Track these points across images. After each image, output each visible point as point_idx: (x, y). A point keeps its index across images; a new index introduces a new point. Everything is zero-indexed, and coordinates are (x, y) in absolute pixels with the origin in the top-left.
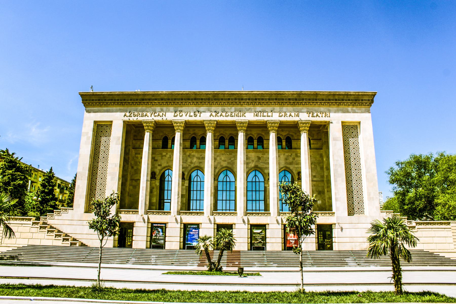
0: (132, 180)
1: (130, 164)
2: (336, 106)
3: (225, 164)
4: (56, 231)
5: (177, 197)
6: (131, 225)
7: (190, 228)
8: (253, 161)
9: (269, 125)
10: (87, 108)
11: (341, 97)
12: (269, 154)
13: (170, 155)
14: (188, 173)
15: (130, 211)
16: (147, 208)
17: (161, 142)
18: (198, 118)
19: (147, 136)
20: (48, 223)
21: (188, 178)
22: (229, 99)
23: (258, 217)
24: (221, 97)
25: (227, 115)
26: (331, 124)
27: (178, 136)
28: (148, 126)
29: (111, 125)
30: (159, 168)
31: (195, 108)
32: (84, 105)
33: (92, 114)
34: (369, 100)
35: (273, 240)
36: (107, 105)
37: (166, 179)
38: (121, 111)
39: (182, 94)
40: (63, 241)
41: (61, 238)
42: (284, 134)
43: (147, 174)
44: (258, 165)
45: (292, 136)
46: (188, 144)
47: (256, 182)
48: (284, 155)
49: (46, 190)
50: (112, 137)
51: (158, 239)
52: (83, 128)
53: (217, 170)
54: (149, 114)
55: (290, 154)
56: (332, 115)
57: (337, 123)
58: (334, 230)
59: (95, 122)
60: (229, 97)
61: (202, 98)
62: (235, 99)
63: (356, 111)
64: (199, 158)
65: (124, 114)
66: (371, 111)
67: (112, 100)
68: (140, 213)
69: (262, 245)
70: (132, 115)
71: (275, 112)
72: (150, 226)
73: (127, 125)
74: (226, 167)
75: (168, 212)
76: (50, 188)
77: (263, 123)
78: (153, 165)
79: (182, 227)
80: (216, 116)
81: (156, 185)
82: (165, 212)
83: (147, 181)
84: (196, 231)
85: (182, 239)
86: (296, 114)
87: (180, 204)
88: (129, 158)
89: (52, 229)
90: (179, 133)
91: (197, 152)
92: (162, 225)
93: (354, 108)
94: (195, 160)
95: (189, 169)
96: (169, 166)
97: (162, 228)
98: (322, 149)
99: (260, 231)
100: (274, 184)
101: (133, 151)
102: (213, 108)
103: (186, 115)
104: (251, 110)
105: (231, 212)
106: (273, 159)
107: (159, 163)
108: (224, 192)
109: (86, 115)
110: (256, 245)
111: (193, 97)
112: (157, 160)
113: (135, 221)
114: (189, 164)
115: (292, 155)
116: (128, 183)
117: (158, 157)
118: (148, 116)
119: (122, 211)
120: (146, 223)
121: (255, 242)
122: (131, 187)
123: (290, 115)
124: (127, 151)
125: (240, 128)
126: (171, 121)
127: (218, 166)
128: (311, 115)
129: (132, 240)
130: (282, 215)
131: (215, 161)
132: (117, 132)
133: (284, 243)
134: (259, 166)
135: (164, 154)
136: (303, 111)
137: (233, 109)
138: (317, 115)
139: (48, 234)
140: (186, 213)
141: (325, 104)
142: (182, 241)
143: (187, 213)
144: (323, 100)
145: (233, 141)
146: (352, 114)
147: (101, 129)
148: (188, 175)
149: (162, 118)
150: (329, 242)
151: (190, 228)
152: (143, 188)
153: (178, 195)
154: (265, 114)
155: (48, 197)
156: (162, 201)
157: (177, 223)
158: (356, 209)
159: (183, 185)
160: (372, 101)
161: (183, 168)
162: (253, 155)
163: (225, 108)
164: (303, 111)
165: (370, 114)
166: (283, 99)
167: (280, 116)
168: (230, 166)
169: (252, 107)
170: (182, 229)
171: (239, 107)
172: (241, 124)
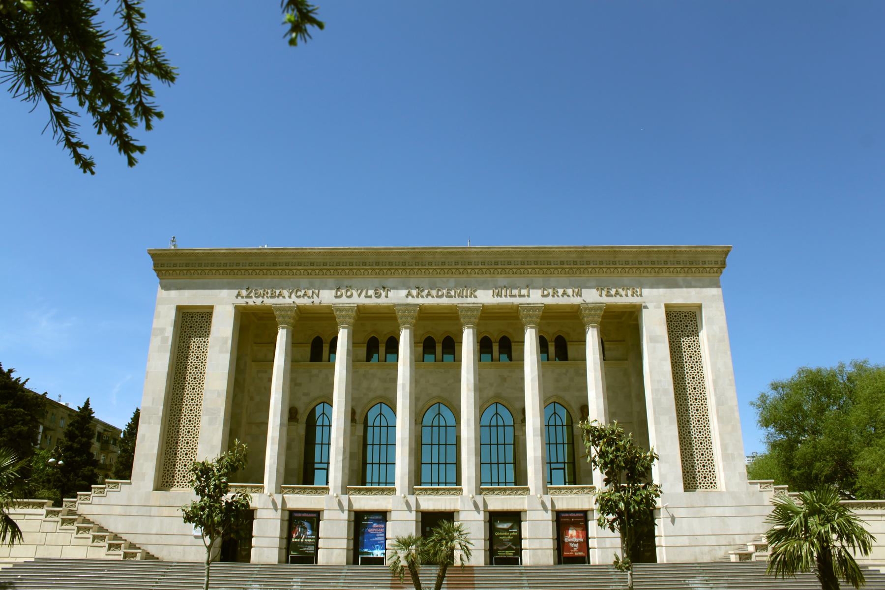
2: (653, 274)
4: (96, 528)
17: (308, 349)
18: (383, 301)
22: (443, 263)
25: (440, 293)
26: (644, 311)
27: (343, 337)
31: (377, 281)
32: (158, 275)
33: (173, 293)
34: (716, 263)
37: (319, 423)
39: (351, 253)
40: (77, 533)
41: (106, 544)
46: (363, 352)
52: (155, 320)
54: (285, 293)
56: (646, 292)
57: (655, 307)
59: (179, 309)
60: (443, 260)
62: (457, 263)
65: (236, 292)
67: (212, 264)
68: (266, 491)
69: (514, 554)
70: (252, 294)
71: (534, 288)
75: (323, 488)
82: (316, 489)
89: (86, 525)
93: (689, 278)
97: (310, 520)
102: (413, 281)
103: (359, 295)
106: (532, 380)
109: (162, 293)
110: (501, 555)
112: (300, 385)
115: (567, 371)
118: (284, 297)
123: (564, 293)
125: (467, 320)
126: (329, 307)
128: (604, 293)
130: (552, 491)
132: (223, 327)
138: (617, 293)
139: (79, 535)
141: (631, 271)
144: (627, 263)
145: (452, 346)
146: (685, 289)
149: (312, 300)
151: (367, 520)
152: (273, 439)
154: (515, 292)
157: (343, 511)
159: (352, 434)
160: (723, 265)
165: (720, 290)
166: (549, 263)
167: (543, 296)
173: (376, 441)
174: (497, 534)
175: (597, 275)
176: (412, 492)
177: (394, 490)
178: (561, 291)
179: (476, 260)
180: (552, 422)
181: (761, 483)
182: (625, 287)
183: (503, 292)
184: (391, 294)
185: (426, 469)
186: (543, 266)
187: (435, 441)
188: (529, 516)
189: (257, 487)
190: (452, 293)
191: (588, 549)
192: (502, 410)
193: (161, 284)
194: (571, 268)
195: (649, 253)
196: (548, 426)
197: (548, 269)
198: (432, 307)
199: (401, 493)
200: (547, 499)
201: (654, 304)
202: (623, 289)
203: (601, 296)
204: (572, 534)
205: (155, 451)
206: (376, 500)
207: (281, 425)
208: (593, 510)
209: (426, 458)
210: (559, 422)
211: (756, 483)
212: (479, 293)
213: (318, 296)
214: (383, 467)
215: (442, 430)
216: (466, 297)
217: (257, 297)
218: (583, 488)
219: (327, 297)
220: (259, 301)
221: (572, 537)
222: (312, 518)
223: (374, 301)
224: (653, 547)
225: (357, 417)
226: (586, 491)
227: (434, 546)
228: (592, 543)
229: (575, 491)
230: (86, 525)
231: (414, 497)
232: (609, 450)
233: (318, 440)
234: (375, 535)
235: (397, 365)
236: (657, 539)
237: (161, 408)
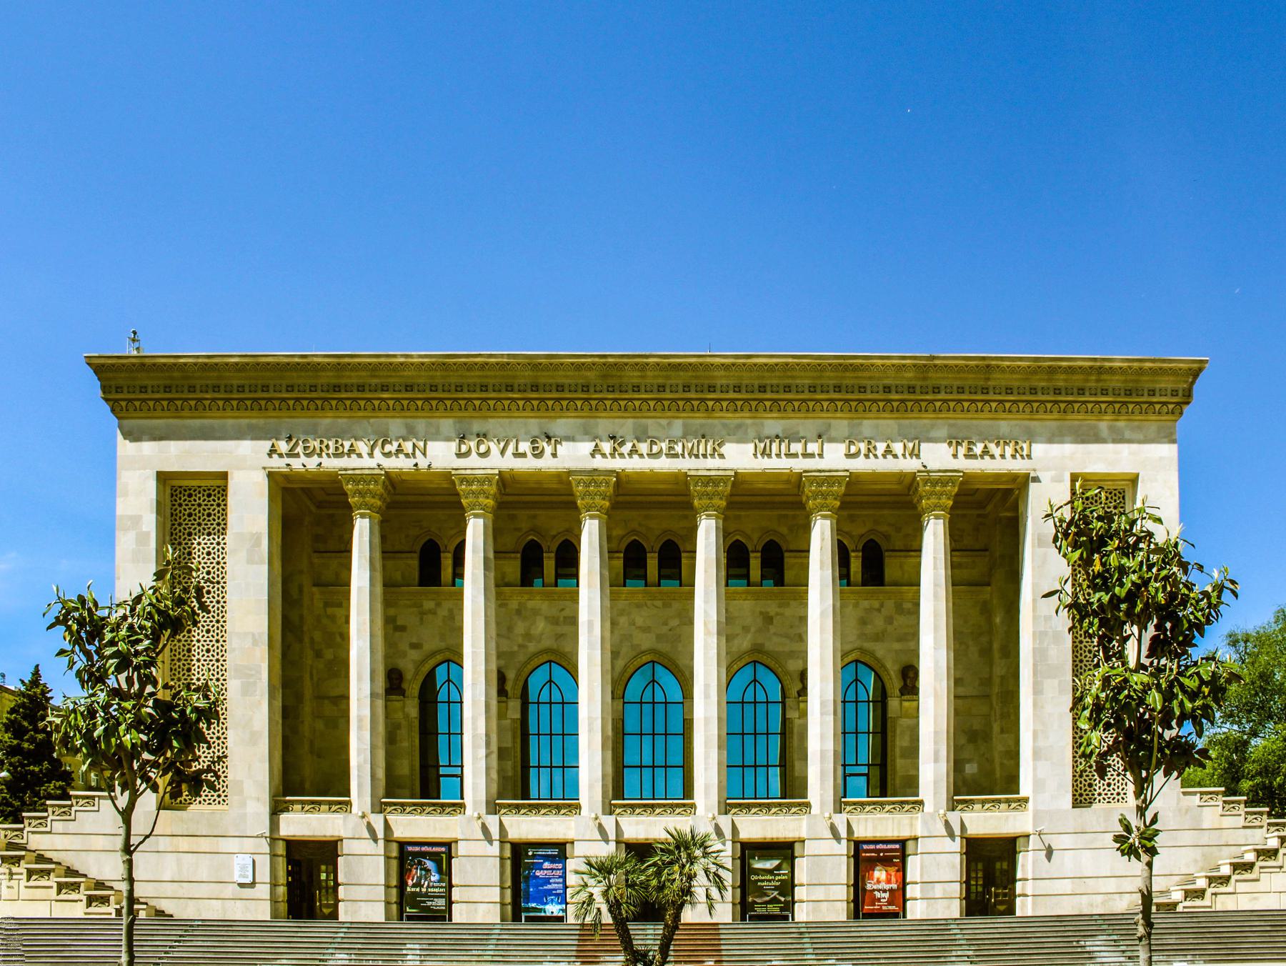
0: (320, 698)
1: (307, 640)
2: (1055, 415)
3: (646, 641)
4: (61, 870)
5: (482, 752)
6: (328, 851)
7: (534, 856)
8: (746, 629)
9: (810, 489)
10: (125, 422)
11: (1077, 380)
12: (806, 605)
13: (451, 611)
14: (518, 676)
15: (320, 803)
16: (381, 791)
17: (414, 563)
18: (547, 463)
19: (362, 532)
20: (29, 847)
21: (519, 692)
22: (661, 388)
24: (633, 377)
25: (655, 449)
26: (1032, 486)
27: (475, 532)
28: (361, 494)
29: (225, 489)
30: (414, 655)
31: (534, 425)
32: (113, 410)
33: (148, 447)
34: (1174, 393)
35: (819, 893)
36: (199, 408)
37: (442, 696)
38: (256, 434)
39: (483, 366)
40: (28, 880)
41: (82, 895)
42: (859, 529)
43: (373, 672)
44: (762, 645)
45: (887, 537)
46: (513, 568)
47: (755, 703)
48: (856, 605)
49: (26, 745)
50: (229, 538)
51: (426, 895)
52: (119, 500)
53: (620, 663)
54: (362, 447)
55: (876, 604)
56: (1039, 449)
58: (1021, 858)
59: (163, 478)
60: (660, 381)
61: (561, 381)
62: (687, 388)
63: (1127, 434)
64: (554, 621)
65: (267, 445)
66: (1177, 436)
67: (216, 388)
68: (355, 809)
69: (782, 909)
70: (299, 449)
71: (831, 440)
72: (395, 853)
73: (285, 490)
74: (652, 651)
75: (454, 805)
76: (40, 736)
77: (788, 482)
78: (390, 643)
79: (508, 854)
80: (613, 455)
81: (407, 716)
82: (443, 805)
83: (373, 695)
84: (554, 866)
85: (508, 893)
86: (910, 445)
87: (494, 775)
88: (301, 617)
89: (42, 866)
90: (481, 521)
91: (548, 597)
92: (436, 849)
93: (1121, 424)
94: (541, 626)
95: (522, 658)
96: (448, 649)
97: (435, 857)
98: (989, 585)
99: (776, 862)
100: (823, 704)
101: (317, 596)
102: (604, 424)
103: (503, 452)
104: (746, 433)
106: (822, 614)
107: (414, 640)
108: (647, 740)
109: (125, 448)
110: (760, 910)
111: (526, 377)
112: (402, 629)
113: (343, 834)
114: (520, 640)
115: (882, 605)
116: (307, 708)
117: (406, 617)
118: (360, 455)
119: (293, 802)
120: (381, 843)
121: (758, 900)
122: (320, 725)
123: (888, 451)
124: (295, 593)
125: (705, 501)
126: (447, 475)
127: (624, 650)
128: (962, 450)
129: (337, 901)
130: (848, 808)
131: (612, 632)
133: (856, 901)
134: (769, 646)
135: (429, 605)
136: (933, 434)
137: (677, 426)
138: (986, 452)
139: (32, 883)
140: (518, 807)
141: (1014, 408)
142: (508, 899)
143: (523, 806)
144: (1009, 391)
145: (675, 560)
146: (1110, 446)
147: (189, 506)
148: (517, 679)
149: (413, 461)
150: (1005, 895)
151: (534, 856)
152: (360, 720)
153: (488, 744)
154: (797, 447)
155: (37, 769)
156: (432, 771)
157: (490, 841)
159: (501, 715)
160: (1188, 394)
161: (499, 656)
162: (747, 607)
163: (650, 421)
164: (933, 434)
165: (1174, 447)
166: (862, 389)
167: (849, 456)
168: (664, 647)
169: (749, 421)
170: (508, 863)
171: (698, 421)
172: (706, 484)
173: (545, 729)
174: (754, 878)
175: (951, 415)
176: (609, 810)
177: (578, 807)
178: (881, 447)
179: (724, 382)
180: (851, 696)
181: (1202, 793)
182: (1001, 440)
183: (775, 446)
184: (564, 449)
185: (631, 777)
186: (849, 396)
187: (647, 728)
188: (810, 847)
189: (340, 803)
190: (679, 448)
191: (905, 901)
193: (120, 427)
194: (902, 401)
195: (1052, 371)
196: (846, 702)
197: (860, 401)
198: (641, 476)
199: (591, 810)
200: (840, 821)
202: (998, 444)
203: (955, 456)
204: (880, 878)
206: (547, 824)
207: (373, 695)
209: (631, 758)
211: (1194, 793)
212: (729, 449)
213: (424, 454)
214: (557, 773)
215: (660, 709)
216: (705, 456)
217: (308, 455)
218: (902, 803)
219: (441, 455)
220: (312, 463)
221: (879, 882)
222: (438, 854)
223: (529, 464)
224: (1012, 897)
225: (509, 687)
226: (907, 807)
227: (658, 874)
228: (911, 891)
229: (888, 808)
230: (42, 866)
231: (612, 818)
232: (1130, 563)
233: (442, 727)
235: (578, 593)
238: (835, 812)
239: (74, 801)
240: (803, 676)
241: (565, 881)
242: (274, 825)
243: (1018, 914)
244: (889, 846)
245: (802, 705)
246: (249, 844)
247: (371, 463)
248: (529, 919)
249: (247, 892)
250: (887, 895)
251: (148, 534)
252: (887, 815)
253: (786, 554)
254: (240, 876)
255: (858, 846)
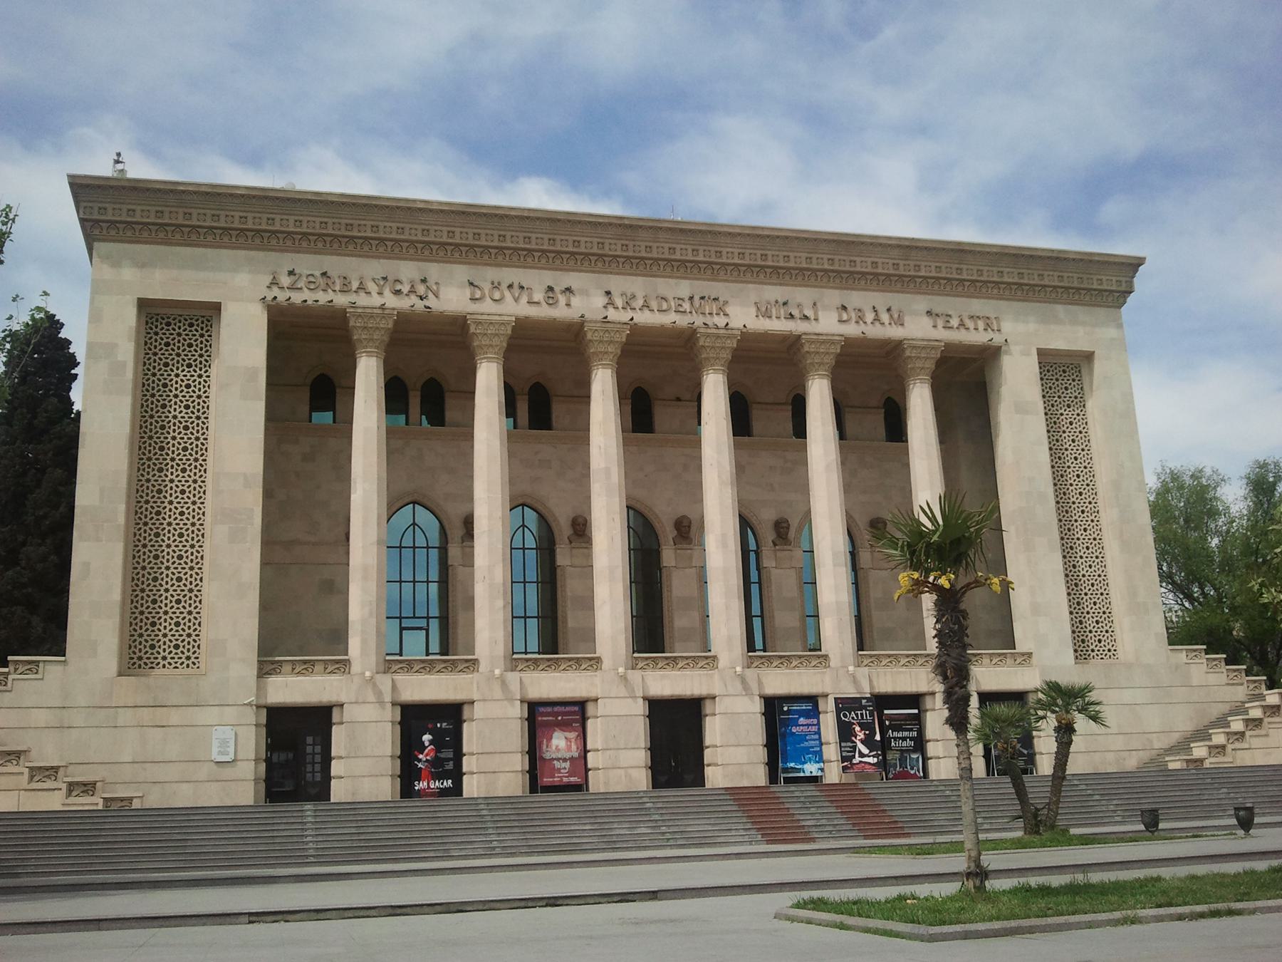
18: (561, 312)
23: (577, 674)
59: (144, 305)
84: (809, 721)
105: (529, 656)
128: (940, 323)
145: (329, 392)
158: (165, 648)
167: (473, 299)
177: (598, 660)
180: (518, 542)
191: (587, 770)
192: (424, 516)
201: (1021, 340)
204: (559, 744)
205: (117, 595)
208: (933, 694)
210: (421, 541)
220: (323, 298)
221: (558, 749)
234: (803, 738)
236: (707, 752)
237: (122, 507)
238: (715, 667)
239: (11, 668)
240: (468, 523)
241: (921, 732)
242: (261, 689)
243: (465, 795)
244: (568, 709)
245: (468, 550)
246: (230, 714)
247: (376, 301)
248: (787, 780)
249: (228, 772)
250: (567, 765)
251: (124, 364)
252: (904, 669)
253: (447, 395)
254: (220, 753)
255: (534, 708)
